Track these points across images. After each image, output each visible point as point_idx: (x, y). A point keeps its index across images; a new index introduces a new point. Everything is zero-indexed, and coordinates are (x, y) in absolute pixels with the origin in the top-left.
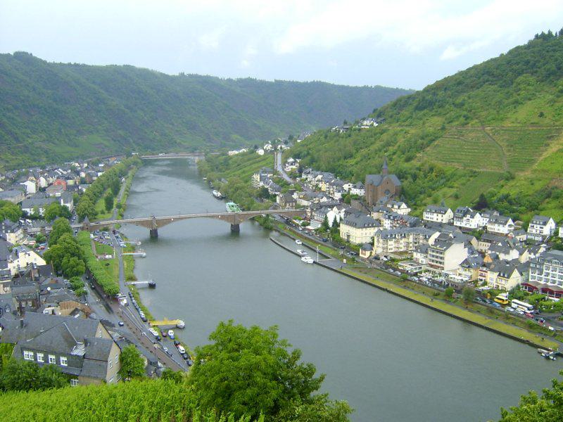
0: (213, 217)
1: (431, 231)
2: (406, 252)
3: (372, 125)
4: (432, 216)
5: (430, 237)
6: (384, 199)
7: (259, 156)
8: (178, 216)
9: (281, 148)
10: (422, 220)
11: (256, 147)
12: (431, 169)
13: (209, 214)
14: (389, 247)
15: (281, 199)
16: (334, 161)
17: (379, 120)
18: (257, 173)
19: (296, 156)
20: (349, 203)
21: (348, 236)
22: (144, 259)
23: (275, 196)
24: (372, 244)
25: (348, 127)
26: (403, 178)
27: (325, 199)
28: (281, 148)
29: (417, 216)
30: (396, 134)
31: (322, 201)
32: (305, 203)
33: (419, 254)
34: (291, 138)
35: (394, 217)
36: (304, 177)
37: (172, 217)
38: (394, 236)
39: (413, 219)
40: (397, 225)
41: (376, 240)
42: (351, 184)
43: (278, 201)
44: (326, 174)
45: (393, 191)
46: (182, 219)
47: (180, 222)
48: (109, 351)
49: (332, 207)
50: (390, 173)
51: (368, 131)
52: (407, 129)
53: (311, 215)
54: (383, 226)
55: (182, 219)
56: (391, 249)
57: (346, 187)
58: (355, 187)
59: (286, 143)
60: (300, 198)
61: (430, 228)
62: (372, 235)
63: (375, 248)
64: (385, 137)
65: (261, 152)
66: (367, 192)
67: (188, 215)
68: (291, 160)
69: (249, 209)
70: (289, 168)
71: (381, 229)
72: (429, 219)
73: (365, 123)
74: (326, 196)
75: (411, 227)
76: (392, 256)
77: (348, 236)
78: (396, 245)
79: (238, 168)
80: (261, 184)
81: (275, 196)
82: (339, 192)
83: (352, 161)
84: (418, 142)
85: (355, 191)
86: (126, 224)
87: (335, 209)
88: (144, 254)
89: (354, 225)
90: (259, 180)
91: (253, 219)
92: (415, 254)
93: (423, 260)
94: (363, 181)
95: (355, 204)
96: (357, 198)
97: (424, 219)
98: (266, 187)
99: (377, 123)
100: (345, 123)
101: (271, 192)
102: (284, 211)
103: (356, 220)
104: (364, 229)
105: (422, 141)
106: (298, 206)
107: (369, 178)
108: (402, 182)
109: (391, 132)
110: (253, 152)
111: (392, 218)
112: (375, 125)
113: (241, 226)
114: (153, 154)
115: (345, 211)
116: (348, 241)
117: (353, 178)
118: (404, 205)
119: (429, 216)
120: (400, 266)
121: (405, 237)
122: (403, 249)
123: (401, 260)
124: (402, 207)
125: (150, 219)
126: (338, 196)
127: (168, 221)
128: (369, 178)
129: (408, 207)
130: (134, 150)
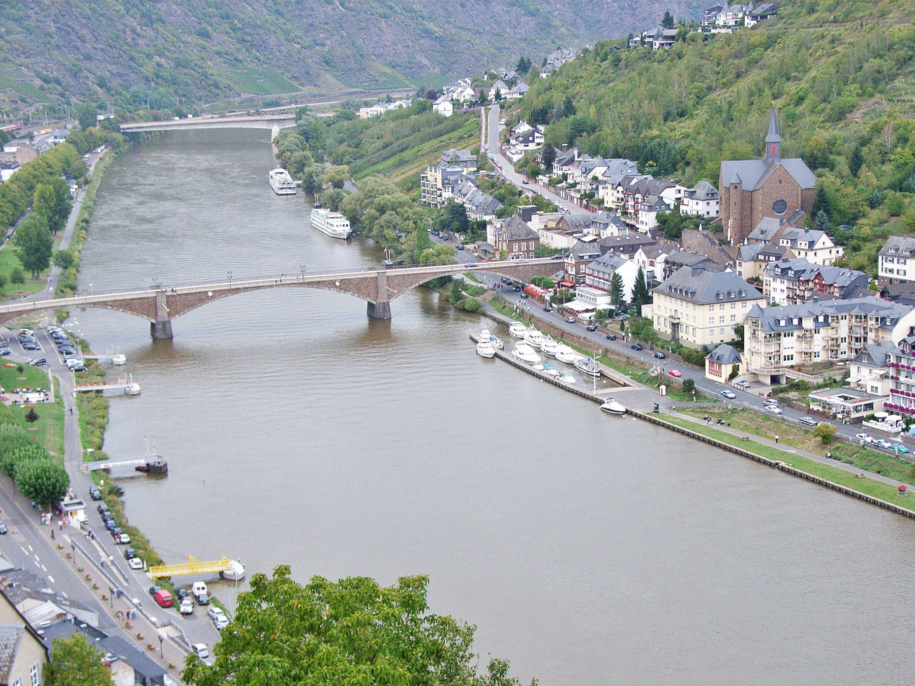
0: (318, 284)
1: (898, 307)
2: (830, 365)
3: (741, 23)
4: (901, 267)
5: (895, 322)
6: (770, 224)
7: (441, 119)
8: (224, 286)
9: (498, 96)
10: (876, 277)
11: (433, 96)
12: (739, 331)
13: (309, 278)
14: (785, 353)
15: (498, 234)
16: (637, 126)
17: (759, 11)
18: (435, 166)
19: (539, 117)
20: (675, 235)
21: (675, 326)
22: (137, 400)
23: (483, 225)
24: (739, 345)
25: (673, 32)
26: (824, 165)
27: (612, 231)
28: (498, 96)
29: (861, 268)
30: (802, 45)
31: (606, 234)
32: (559, 241)
33: (865, 371)
34: (523, 66)
35: (798, 273)
36: (557, 172)
37: (209, 288)
38: (795, 322)
39: (847, 277)
40: (807, 294)
41: (747, 334)
42: (683, 189)
43: (491, 239)
44: (616, 163)
45: (793, 201)
46: (237, 290)
47: (231, 298)
48: (12, 657)
49: (631, 250)
50: (785, 154)
51: (728, 40)
52: (835, 30)
53: (577, 272)
54: (767, 298)
55: (237, 290)
56: (790, 358)
57: (669, 196)
58: (692, 195)
59: (511, 84)
60: (546, 228)
61: (895, 298)
62: (739, 320)
63: (746, 356)
64: (772, 57)
65: (444, 107)
66: (726, 206)
67: (253, 283)
68: (524, 128)
69: (415, 263)
70: (518, 151)
71: (763, 304)
72: (894, 276)
73: (721, 20)
74: (616, 221)
75: (844, 297)
76: (796, 376)
77: (675, 326)
78: (804, 347)
79: (385, 153)
80: (447, 194)
81: (483, 225)
82: (651, 208)
83: (686, 126)
84: (866, 66)
85: (692, 207)
86: (83, 307)
87: (640, 255)
88: (135, 388)
89: (688, 296)
90: (440, 185)
91: (426, 288)
92: (853, 369)
93: (878, 384)
94: (715, 179)
95: (692, 238)
96: (698, 221)
97: (880, 274)
98: (458, 201)
99: (754, 18)
100: (668, 22)
101: (473, 216)
102: (504, 264)
103: (693, 283)
104: (717, 306)
105: (877, 61)
106: (542, 251)
107: (730, 171)
108: (820, 176)
109: (791, 40)
110: (423, 109)
111: (791, 273)
112: (749, 22)
113: (395, 305)
114: (156, 119)
115: (666, 262)
116: (675, 338)
117: (689, 170)
118: (824, 240)
119: (895, 266)
120: (814, 400)
121: (826, 323)
122: (823, 357)
123: (819, 387)
124: (818, 245)
125: (151, 293)
126: (648, 221)
127: (200, 298)
128: (730, 171)
129: (837, 243)
130: (102, 107)
